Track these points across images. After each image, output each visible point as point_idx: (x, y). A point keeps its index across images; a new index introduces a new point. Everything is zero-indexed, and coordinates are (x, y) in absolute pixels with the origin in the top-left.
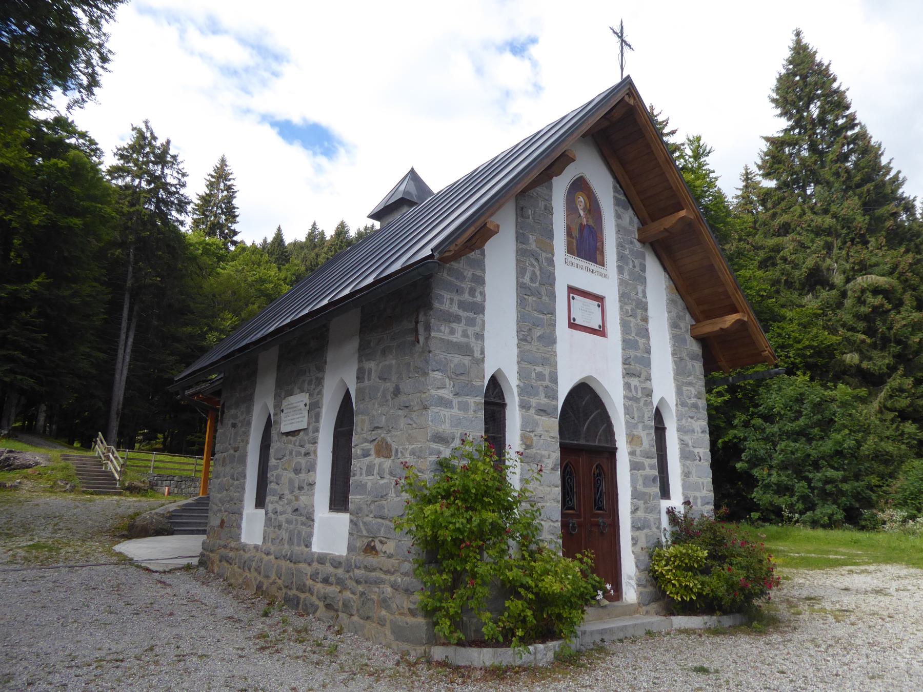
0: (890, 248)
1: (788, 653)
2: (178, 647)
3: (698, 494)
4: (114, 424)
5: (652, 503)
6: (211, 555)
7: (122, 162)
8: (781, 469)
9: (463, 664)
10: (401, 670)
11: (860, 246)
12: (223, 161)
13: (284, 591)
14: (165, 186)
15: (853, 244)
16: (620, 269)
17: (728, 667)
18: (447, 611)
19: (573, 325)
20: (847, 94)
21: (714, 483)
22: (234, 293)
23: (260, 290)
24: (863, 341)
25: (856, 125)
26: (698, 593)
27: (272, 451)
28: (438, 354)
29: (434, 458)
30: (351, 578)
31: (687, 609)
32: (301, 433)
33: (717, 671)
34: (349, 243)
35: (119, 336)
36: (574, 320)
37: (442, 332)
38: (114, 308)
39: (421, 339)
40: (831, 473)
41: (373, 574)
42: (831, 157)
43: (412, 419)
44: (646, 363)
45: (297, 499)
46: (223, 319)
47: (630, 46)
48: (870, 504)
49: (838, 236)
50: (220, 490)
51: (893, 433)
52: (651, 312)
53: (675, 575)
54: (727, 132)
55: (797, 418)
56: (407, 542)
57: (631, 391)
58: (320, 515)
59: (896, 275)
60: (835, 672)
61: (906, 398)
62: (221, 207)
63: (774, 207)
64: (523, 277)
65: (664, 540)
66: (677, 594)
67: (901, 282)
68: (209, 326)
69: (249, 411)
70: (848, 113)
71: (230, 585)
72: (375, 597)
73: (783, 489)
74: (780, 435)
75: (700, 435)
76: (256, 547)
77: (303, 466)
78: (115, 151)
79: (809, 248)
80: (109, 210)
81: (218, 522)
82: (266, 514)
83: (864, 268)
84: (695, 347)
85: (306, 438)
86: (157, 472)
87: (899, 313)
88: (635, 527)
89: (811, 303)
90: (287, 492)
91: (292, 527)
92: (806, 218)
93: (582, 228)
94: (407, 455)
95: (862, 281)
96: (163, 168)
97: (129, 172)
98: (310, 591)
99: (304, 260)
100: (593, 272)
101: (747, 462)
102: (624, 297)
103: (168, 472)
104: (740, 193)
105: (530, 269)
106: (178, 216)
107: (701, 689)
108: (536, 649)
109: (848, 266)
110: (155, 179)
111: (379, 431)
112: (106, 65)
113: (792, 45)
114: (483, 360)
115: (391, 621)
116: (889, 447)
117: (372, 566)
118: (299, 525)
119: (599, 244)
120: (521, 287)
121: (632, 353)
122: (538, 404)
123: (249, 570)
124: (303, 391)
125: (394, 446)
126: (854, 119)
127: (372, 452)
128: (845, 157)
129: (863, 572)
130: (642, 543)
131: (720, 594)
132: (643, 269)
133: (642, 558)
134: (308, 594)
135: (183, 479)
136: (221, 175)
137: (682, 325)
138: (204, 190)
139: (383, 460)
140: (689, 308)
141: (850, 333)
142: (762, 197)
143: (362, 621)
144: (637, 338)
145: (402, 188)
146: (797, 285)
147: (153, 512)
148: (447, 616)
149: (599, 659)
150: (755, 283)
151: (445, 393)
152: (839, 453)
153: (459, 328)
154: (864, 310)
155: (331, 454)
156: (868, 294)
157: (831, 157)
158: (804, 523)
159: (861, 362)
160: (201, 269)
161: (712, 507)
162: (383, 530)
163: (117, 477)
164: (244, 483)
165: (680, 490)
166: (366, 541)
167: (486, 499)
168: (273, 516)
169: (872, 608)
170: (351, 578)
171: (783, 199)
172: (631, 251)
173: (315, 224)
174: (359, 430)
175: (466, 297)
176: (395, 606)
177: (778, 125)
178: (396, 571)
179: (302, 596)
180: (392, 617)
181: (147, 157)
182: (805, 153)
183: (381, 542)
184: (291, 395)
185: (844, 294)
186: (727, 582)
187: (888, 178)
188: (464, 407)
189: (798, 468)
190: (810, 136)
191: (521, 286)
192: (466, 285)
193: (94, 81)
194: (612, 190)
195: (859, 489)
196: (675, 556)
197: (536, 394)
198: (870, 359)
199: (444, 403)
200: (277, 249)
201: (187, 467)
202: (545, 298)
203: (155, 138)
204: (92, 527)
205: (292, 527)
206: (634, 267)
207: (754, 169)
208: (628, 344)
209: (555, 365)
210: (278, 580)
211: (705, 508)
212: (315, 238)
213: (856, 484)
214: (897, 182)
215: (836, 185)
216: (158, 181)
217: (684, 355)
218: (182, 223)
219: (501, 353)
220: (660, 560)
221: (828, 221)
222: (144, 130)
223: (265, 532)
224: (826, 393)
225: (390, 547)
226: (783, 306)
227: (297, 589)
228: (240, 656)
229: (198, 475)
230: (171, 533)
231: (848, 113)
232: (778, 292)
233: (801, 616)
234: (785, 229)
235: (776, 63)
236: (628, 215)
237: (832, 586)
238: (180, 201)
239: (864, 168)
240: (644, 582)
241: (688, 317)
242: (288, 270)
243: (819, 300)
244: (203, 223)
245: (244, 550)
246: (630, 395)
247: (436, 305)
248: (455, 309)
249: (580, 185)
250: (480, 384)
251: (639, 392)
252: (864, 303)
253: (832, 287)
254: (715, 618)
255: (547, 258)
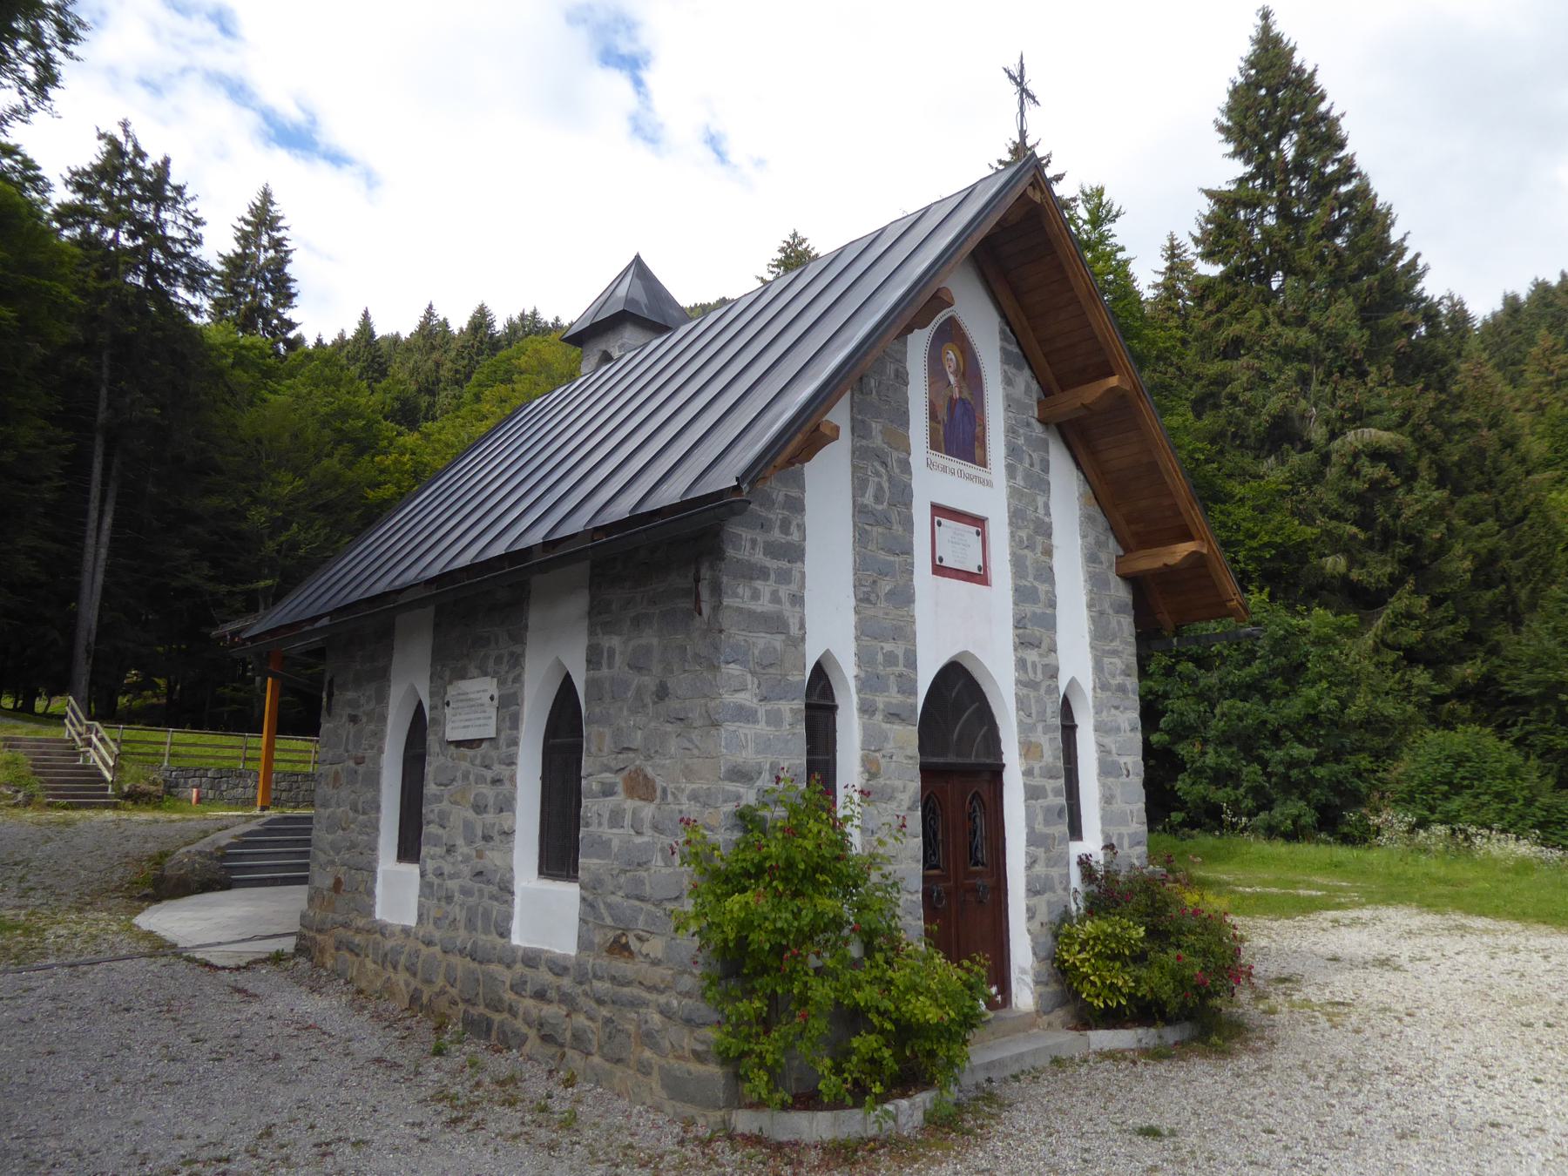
0: (1401, 382)
1: (1272, 1094)
2: (312, 1127)
3: (1124, 830)
4: (82, 671)
5: (1057, 849)
6: (319, 937)
7: (80, 196)
8: (1221, 744)
9: (785, 1139)
10: (690, 1155)
11: (1353, 380)
12: (266, 197)
13: (461, 1006)
14: (163, 242)
15: (1342, 376)
16: (1011, 471)
17: (1188, 1122)
18: (761, 1056)
19: (939, 569)
20: (1342, 122)
21: (1147, 810)
22: (295, 436)
23: (340, 430)
24: (1353, 537)
25: (1355, 175)
26: (1130, 995)
27: (429, 770)
28: (735, 634)
29: (730, 807)
30: (586, 994)
31: (1111, 1019)
32: (484, 745)
33: (1173, 1133)
34: (495, 344)
35: (85, 513)
36: (941, 560)
37: (739, 597)
38: (78, 465)
39: (706, 609)
40: (1299, 751)
41: (626, 990)
42: (1312, 229)
43: (691, 741)
44: (1049, 623)
45: (480, 855)
46: (276, 484)
47: (1033, 98)
48: (1356, 800)
49: (1319, 361)
50: (331, 829)
51: (1396, 687)
52: (1056, 540)
53: (1095, 969)
54: (1154, 188)
55: (1248, 663)
56: (688, 944)
57: (1026, 671)
58: (524, 884)
59: (1407, 428)
60: (1346, 1129)
61: (1417, 628)
62: (264, 279)
63: (1218, 310)
64: (863, 495)
65: (1074, 907)
66: (1098, 996)
67: (1415, 440)
68: (250, 494)
69: (382, 698)
70: (1342, 154)
71: (360, 992)
72: (631, 1028)
73: (1222, 777)
74: (1220, 689)
75: (1129, 734)
76: (406, 931)
77: (491, 801)
78: (68, 176)
79: (1274, 381)
80: (65, 290)
81: (330, 882)
82: (423, 875)
83: (1359, 417)
84: (1122, 593)
85: (494, 753)
86: (176, 763)
87: (1410, 491)
88: (1032, 891)
89: (1274, 472)
90: (460, 842)
91: (472, 901)
92: (1270, 330)
93: (952, 403)
94: (684, 800)
95: (1356, 437)
96: (157, 210)
97: (95, 215)
98: (512, 1011)
99: (415, 371)
100: (970, 478)
101: (1167, 732)
102: (1016, 517)
103: (197, 763)
104: (1160, 279)
105: (873, 480)
106: (189, 297)
107: (1154, 1168)
108: (897, 1108)
109: (1333, 413)
110: (141, 228)
111: (631, 755)
112: (71, 48)
113: (1254, 34)
114: (803, 639)
115: (661, 1068)
116: (1389, 708)
117: (624, 977)
118: (486, 899)
119: (978, 429)
120: (860, 511)
121: (1029, 609)
122: (887, 705)
123: (395, 968)
124: (486, 674)
125: (660, 783)
126: (1352, 166)
127: (620, 788)
128: (1334, 230)
129: (1355, 922)
130: (1043, 915)
131: (1164, 997)
132: (1046, 468)
133: (1042, 940)
134: (505, 1015)
135: (223, 774)
136: (263, 219)
137: (1103, 556)
138: (231, 247)
139: (639, 803)
140: (1114, 529)
141: (1334, 523)
142: (1199, 293)
143: (608, 1066)
144: (1036, 584)
145: (622, 291)
146: (1251, 441)
147: (193, 848)
148: (762, 1065)
149: (992, 1116)
150: (1187, 439)
151: (746, 698)
152: (1313, 719)
153: (765, 588)
154: (1356, 485)
155: (539, 784)
156: (1364, 460)
157: (1312, 229)
158: (1255, 830)
159: (1349, 570)
160: (233, 393)
161: (1145, 849)
162: (642, 918)
163: (108, 776)
164: (378, 820)
165: (1098, 825)
166: (611, 935)
167: (821, 878)
168: (436, 881)
169: (1380, 997)
170: (586, 994)
171: (1234, 296)
172: (1028, 439)
173: (431, 307)
174: (594, 749)
175: (776, 535)
176: (667, 1044)
177: (1228, 171)
178: (667, 988)
179: (497, 1018)
180: (663, 1062)
181: (128, 189)
182: (1270, 221)
183: (640, 939)
184: (463, 677)
185: (1325, 459)
186: (1173, 978)
187: (1400, 264)
188: (774, 719)
189: (1247, 742)
190: (1280, 194)
191: (860, 510)
192: (776, 515)
193: (47, 78)
194: (997, 337)
195: (1341, 776)
196: (1096, 938)
197: (885, 689)
198: (1364, 565)
199: (744, 714)
200: (367, 352)
201: (228, 752)
202: (898, 529)
203: (142, 155)
204: (89, 883)
205: (472, 901)
206: (1032, 465)
207: (1191, 251)
208: (1022, 594)
209: (911, 638)
210: (448, 988)
211: (1134, 855)
212: (431, 332)
213: (1336, 768)
214: (1413, 272)
215: (1318, 276)
216: (152, 233)
217: (1106, 605)
218: (197, 310)
219: (830, 626)
220: (1071, 944)
221: (1305, 336)
222: (121, 138)
223: (421, 906)
224: (1294, 622)
225: (655, 947)
226: (1230, 476)
227: (487, 1006)
228: (422, 1140)
229: (250, 765)
230: (227, 885)
231: (1342, 154)
232: (1221, 452)
233: (1276, 1017)
234: (1234, 348)
235: (1227, 63)
236: (1024, 378)
237: (1312, 952)
238: (192, 270)
239: (1363, 249)
240: (1044, 979)
241: (1112, 542)
242: (385, 391)
243: (1286, 469)
244: (232, 308)
245: (383, 934)
246: (1024, 678)
247: (730, 552)
248: (759, 557)
249: (952, 334)
250: (798, 678)
251: (1039, 672)
252: (1357, 474)
253: (1307, 446)
254: (1153, 1031)
255: (899, 461)
